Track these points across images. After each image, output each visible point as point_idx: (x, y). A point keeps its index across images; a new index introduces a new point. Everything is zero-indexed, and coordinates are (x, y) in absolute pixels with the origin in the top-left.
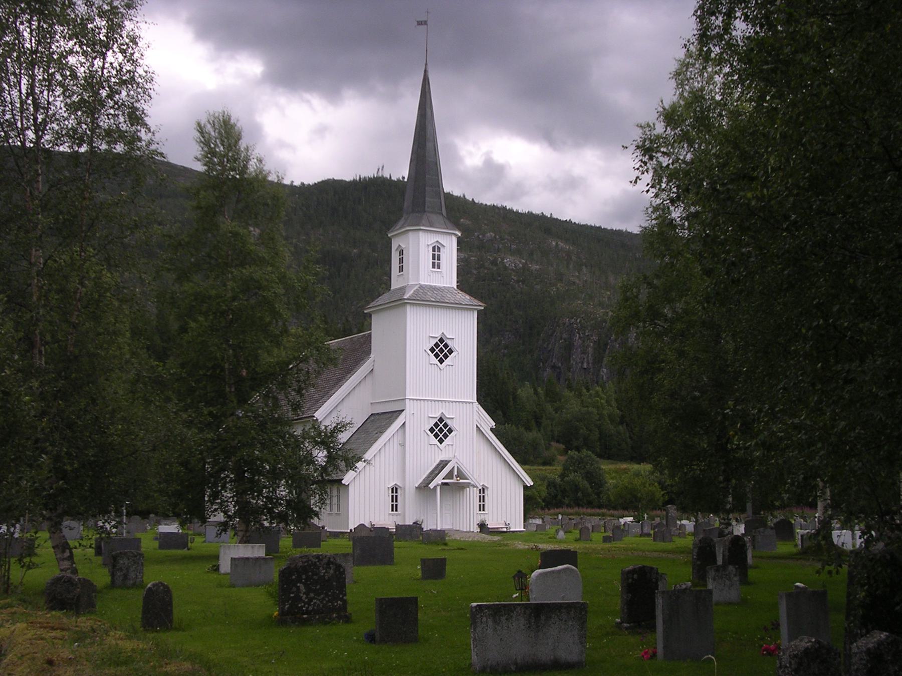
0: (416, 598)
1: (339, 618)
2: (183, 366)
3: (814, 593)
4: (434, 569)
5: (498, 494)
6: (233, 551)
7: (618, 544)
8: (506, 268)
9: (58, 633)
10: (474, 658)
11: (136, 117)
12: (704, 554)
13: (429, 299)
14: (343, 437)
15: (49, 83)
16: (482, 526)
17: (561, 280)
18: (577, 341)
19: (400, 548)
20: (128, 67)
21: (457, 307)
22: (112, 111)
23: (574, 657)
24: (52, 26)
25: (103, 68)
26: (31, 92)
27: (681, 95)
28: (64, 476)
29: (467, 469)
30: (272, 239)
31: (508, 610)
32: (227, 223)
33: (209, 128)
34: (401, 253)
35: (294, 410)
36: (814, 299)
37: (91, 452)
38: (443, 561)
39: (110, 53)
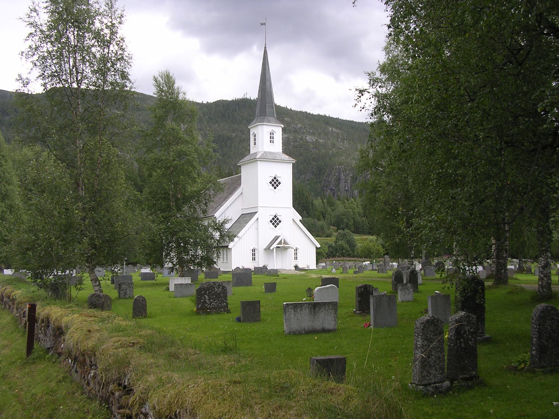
0: (259, 301)
1: (225, 311)
2: (150, 193)
3: (444, 296)
4: (271, 288)
5: (302, 251)
6: (176, 280)
7: (361, 275)
8: (307, 142)
9: (93, 319)
10: (285, 328)
11: (124, 76)
12: (398, 278)
13: (268, 158)
14: (227, 226)
15: (83, 60)
16: (296, 267)
17: (334, 147)
18: (343, 177)
19: (255, 278)
20: (120, 52)
21: (283, 161)
22: (113, 73)
23: (331, 327)
24: (83, 33)
25: (108, 53)
26: (75, 65)
27: (388, 58)
28: (95, 247)
29: (288, 241)
30: (191, 131)
31: (301, 305)
32: (170, 123)
33: (160, 79)
34: (255, 136)
35: (204, 213)
36: (437, 160)
37: (107, 235)
38: (275, 284)
39: (111, 46)
